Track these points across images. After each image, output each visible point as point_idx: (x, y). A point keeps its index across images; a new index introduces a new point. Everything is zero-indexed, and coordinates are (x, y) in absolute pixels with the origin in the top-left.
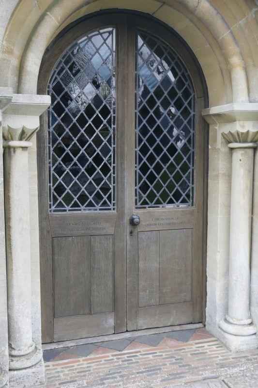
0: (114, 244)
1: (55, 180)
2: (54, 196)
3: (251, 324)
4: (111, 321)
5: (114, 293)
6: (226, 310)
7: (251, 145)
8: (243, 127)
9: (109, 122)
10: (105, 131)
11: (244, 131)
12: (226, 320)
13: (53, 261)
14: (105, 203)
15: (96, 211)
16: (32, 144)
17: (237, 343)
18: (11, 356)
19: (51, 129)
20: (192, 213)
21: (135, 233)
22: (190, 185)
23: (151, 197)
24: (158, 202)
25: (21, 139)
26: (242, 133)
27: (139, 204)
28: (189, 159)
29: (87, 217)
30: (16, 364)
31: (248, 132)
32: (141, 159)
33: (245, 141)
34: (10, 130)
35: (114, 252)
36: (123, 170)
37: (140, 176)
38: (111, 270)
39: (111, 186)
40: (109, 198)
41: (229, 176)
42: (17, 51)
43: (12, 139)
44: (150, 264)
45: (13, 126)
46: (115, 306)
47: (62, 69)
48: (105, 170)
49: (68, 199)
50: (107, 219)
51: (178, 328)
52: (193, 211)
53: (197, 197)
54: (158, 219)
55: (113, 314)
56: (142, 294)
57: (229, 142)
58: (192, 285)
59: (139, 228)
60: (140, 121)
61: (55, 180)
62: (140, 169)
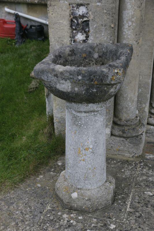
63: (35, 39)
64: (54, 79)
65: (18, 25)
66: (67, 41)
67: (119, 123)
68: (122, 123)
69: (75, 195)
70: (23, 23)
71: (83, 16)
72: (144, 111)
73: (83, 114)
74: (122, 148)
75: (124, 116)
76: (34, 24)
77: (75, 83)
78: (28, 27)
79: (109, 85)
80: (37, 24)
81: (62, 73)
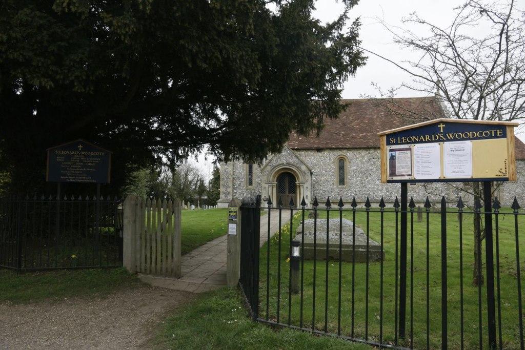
16: (276, 187)
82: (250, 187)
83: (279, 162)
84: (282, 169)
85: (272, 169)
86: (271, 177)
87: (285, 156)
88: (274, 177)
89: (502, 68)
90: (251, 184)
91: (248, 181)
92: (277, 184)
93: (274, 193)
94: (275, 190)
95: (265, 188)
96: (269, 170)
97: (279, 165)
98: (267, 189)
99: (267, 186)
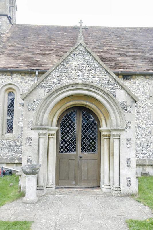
0: (75, 162)
1: (61, 145)
2: (61, 149)
3: (110, 186)
4: (74, 183)
5: (75, 175)
6: (104, 183)
7: (108, 137)
8: (105, 133)
9: (75, 131)
10: (74, 134)
11: (105, 134)
12: (104, 185)
13: (60, 165)
14: (73, 152)
15: (71, 153)
16: (55, 137)
17: (104, 190)
18: (47, 185)
19: (61, 133)
20: (97, 155)
21: (81, 159)
22: (96, 148)
23: (85, 150)
24: (87, 152)
25: (51, 136)
26: (105, 135)
27: (82, 152)
28: (96, 141)
29: (68, 155)
30: (48, 186)
31: (106, 134)
32: (83, 141)
33: (107, 137)
34: (49, 134)
35: (75, 164)
36: (78, 143)
37: (83, 145)
38: (74, 169)
39: (75, 147)
40: (74, 150)
41: (104, 145)
42: (52, 118)
43: (50, 136)
44: (85, 168)
45: (50, 133)
46: (75, 178)
47: (64, 119)
48: (73, 143)
49: (64, 150)
50: (73, 155)
51: (93, 187)
52: (97, 155)
53: (98, 150)
54: (87, 156)
55: (74, 181)
56: (82, 176)
57: (104, 137)
58: (97, 175)
59: (82, 158)
60: (83, 131)
61: (61, 145)
62: (83, 143)
63: (8, 175)
64: (25, 169)
65: (2, 170)
66: (26, 164)
67: (39, 186)
68: (40, 186)
69: (28, 200)
70: (4, 170)
71: (30, 159)
72: (45, 184)
73: (31, 178)
74: (39, 193)
75: (40, 184)
76: (8, 170)
77: (30, 169)
78: (6, 171)
79: (36, 169)
80: (9, 170)
81: (27, 167)
82: (9, 135)
83: (66, 81)
84: (63, 99)
85: (49, 96)
86: (46, 115)
87: (79, 69)
88: (52, 113)
89: (98, 203)
90: (10, 129)
91: (5, 126)
92: (57, 132)
93: (41, 151)
94: (53, 142)
95: (30, 139)
96: (42, 97)
97: (65, 87)
98: (35, 142)
99: (35, 134)
